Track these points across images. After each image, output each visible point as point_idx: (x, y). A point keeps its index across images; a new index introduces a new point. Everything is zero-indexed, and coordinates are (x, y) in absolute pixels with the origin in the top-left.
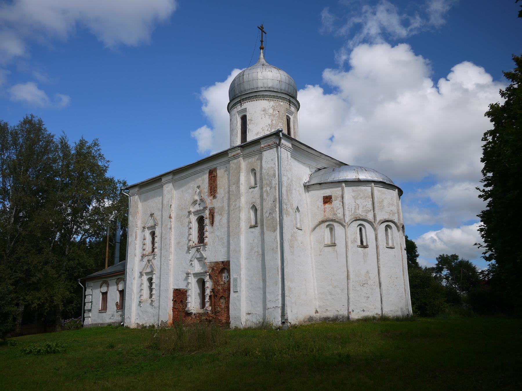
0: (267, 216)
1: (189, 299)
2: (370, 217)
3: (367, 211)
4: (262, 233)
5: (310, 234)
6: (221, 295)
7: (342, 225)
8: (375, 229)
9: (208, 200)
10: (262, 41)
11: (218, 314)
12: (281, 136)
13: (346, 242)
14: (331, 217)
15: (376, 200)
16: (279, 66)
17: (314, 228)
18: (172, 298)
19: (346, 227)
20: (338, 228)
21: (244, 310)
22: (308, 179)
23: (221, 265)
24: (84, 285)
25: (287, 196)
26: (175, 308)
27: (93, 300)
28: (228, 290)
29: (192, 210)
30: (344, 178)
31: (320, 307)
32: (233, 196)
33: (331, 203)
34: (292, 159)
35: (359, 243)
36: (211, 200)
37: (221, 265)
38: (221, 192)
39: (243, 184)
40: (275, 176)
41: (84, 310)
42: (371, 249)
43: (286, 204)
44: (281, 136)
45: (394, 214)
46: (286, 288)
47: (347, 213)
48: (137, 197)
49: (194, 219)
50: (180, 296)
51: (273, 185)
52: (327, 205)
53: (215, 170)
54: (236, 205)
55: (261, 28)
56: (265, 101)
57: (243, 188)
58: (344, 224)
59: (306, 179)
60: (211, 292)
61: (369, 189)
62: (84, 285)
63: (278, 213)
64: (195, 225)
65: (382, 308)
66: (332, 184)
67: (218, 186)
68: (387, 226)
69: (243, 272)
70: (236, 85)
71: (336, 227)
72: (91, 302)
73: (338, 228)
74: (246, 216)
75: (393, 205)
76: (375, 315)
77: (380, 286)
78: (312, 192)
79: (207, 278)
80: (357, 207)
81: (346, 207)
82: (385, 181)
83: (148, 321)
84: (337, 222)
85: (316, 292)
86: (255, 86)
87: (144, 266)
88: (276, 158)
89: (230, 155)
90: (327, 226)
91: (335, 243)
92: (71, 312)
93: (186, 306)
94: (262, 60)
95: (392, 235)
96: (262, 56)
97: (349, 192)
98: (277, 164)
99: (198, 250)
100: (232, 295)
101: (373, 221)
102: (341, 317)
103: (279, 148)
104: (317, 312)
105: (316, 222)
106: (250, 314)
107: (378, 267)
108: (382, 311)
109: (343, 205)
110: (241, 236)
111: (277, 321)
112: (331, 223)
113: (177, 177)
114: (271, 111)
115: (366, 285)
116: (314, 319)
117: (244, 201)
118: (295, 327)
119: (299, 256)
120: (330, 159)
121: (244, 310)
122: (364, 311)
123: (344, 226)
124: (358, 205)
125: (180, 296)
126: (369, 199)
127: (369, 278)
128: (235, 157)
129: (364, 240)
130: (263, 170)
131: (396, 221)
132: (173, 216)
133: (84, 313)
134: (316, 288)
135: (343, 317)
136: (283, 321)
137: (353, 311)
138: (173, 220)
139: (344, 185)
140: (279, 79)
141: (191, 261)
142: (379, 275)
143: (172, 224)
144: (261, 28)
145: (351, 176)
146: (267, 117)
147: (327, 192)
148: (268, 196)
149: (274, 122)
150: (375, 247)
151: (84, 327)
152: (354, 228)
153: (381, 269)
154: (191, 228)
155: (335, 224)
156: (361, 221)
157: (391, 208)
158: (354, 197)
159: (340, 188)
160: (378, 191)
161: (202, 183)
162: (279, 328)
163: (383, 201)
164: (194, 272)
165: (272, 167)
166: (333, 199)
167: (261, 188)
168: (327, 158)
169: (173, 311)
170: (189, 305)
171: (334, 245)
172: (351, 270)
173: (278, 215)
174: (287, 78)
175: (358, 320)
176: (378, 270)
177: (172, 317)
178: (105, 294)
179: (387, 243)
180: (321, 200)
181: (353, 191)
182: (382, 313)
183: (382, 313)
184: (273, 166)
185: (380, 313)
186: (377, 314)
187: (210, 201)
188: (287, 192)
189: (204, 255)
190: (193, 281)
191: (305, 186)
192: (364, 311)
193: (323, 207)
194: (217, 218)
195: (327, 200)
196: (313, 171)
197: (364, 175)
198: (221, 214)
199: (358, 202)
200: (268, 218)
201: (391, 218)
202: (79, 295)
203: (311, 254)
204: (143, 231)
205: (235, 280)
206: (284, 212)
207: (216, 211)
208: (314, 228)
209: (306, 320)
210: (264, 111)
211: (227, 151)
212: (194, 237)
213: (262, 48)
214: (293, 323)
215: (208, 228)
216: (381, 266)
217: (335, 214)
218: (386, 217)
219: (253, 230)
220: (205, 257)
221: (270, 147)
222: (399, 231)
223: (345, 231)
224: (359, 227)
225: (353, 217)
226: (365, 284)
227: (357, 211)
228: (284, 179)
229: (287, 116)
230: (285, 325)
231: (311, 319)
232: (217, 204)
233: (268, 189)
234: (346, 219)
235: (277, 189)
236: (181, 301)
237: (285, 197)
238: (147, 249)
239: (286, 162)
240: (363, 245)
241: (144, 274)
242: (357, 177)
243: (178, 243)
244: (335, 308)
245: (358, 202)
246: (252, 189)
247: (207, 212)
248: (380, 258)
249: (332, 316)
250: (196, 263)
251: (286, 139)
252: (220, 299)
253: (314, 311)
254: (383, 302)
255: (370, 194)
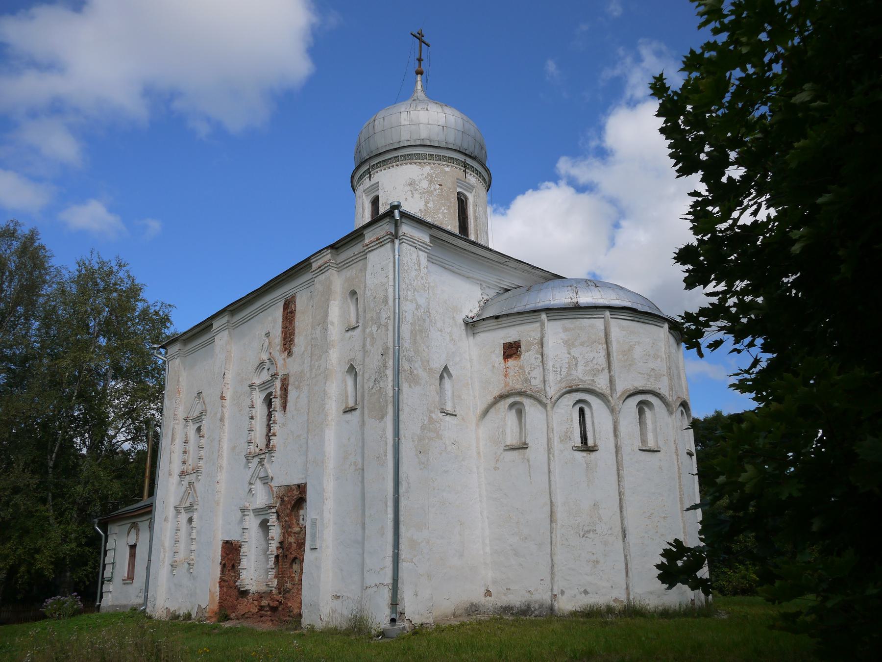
0: (372, 385)
1: (244, 563)
2: (602, 384)
3: (596, 372)
4: (363, 424)
5: (477, 425)
6: (293, 556)
7: (540, 402)
8: (612, 411)
9: (280, 357)
10: (420, 60)
11: (287, 595)
12: (397, 217)
13: (549, 440)
14: (519, 387)
15: (614, 347)
16: (436, 96)
17: (486, 412)
18: (219, 558)
19: (549, 408)
20: (532, 410)
21: (329, 592)
22: (476, 310)
23: (295, 492)
24: (105, 532)
25: (415, 342)
26: (224, 581)
27: (117, 561)
28: (301, 545)
29: (258, 382)
30: (547, 303)
31: (495, 582)
32: (321, 347)
33: (519, 356)
34: (434, 268)
35: (577, 441)
36: (284, 359)
37: (295, 492)
38: (300, 342)
39: (336, 323)
40: (386, 301)
41: (103, 578)
42: (605, 456)
43: (409, 360)
44: (397, 217)
45: (658, 377)
46: (403, 542)
47: (551, 377)
48: (177, 361)
49: (259, 398)
50: (231, 552)
51: (383, 321)
52: (511, 362)
53: (293, 298)
54: (319, 366)
55: (419, 37)
56: (414, 166)
57: (335, 331)
58: (545, 400)
59: (471, 308)
60: (278, 548)
61: (599, 324)
62: (105, 532)
63: (390, 378)
64: (260, 410)
65: (627, 588)
66: (520, 318)
67: (297, 331)
68: (642, 404)
69: (329, 505)
70: (363, 140)
71: (527, 408)
72: (113, 563)
73: (532, 410)
74: (337, 389)
75: (656, 357)
76: (613, 604)
77: (624, 537)
78: (482, 335)
79: (273, 518)
80: (574, 362)
81: (550, 364)
82: (635, 307)
83: (181, 605)
84: (530, 396)
85: (488, 549)
86: (395, 140)
87: (181, 495)
88: (391, 265)
89: (315, 266)
90: (511, 406)
91: (525, 443)
92: (84, 582)
93: (238, 576)
94: (420, 94)
95: (654, 422)
96: (419, 87)
97: (555, 333)
98: (391, 277)
99: (261, 462)
100: (308, 556)
101: (607, 392)
102: (537, 606)
103: (397, 242)
104: (488, 593)
105: (490, 399)
106: (339, 597)
107: (620, 494)
108: (628, 594)
109: (542, 361)
110: (327, 431)
111: (380, 618)
112: (518, 399)
113: (237, 318)
114: (425, 184)
115: (591, 535)
116: (482, 609)
117: (335, 358)
118: (418, 631)
119: (446, 472)
120: (528, 268)
121: (329, 592)
122: (586, 592)
123: (544, 405)
124: (575, 358)
125: (231, 552)
126: (600, 346)
127: (600, 519)
128: (322, 269)
129: (590, 435)
130: (367, 292)
131: (664, 392)
132: (228, 395)
133: (103, 583)
134: (487, 541)
135: (541, 606)
136: (393, 616)
137: (563, 592)
138: (227, 403)
139: (544, 316)
140: (442, 121)
141: (250, 484)
142: (621, 512)
143: (225, 410)
144: (419, 37)
145: (561, 297)
146: (417, 195)
147: (511, 334)
148: (372, 344)
149: (430, 205)
150: (614, 450)
151: (103, 611)
152: (566, 410)
153: (627, 498)
154: (252, 418)
155: (526, 402)
156: (581, 394)
157: (651, 365)
158: (566, 343)
159: (538, 324)
160: (620, 328)
161: (273, 327)
162: (383, 634)
163: (631, 349)
164: (254, 507)
165: (382, 284)
166: (523, 347)
167: (364, 331)
168: (522, 266)
169: (221, 587)
170: (244, 575)
171: (524, 447)
172: (559, 500)
173: (390, 384)
174: (460, 121)
175: (574, 614)
176: (620, 500)
177: (218, 598)
178: (133, 547)
179: (644, 441)
180: (500, 351)
181: (565, 330)
182: (629, 599)
183: (629, 599)
184: (384, 280)
185: (623, 597)
186: (616, 600)
187: (282, 362)
188: (413, 334)
189: (269, 471)
190: (252, 523)
191: (467, 324)
192: (586, 592)
193: (503, 365)
194: (292, 394)
195: (512, 350)
196: (492, 293)
197: (590, 294)
198: (298, 388)
199: (575, 352)
200: (383, 389)
201: (649, 387)
202: (95, 547)
203: (478, 468)
204: (186, 426)
205: (314, 523)
206: (402, 376)
207: (291, 380)
208: (486, 412)
209: (458, 612)
210: (410, 184)
211: (309, 258)
212: (258, 435)
213: (420, 73)
214: (417, 620)
215: (278, 416)
216: (627, 493)
217: (527, 380)
218: (640, 384)
219: (348, 416)
220: (270, 475)
221: (380, 242)
222: (671, 413)
223: (547, 417)
224: (577, 408)
225: (563, 385)
226: (589, 532)
227: (574, 372)
228: (408, 308)
229: (459, 193)
230: (400, 625)
231: (473, 609)
232: (291, 366)
233: (374, 328)
234: (548, 389)
235: (391, 328)
236: (233, 566)
237: (406, 344)
238: (190, 462)
239: (414, 273)
240: (585, 446)
241: (183, 511)
242: (575, 300)
243: (233, 448)
244: (525, 587)
245: (575, 352)
246: (350, 333)
247: (278, 384)
248: (625, 472)
249: (518, 604)
250: (259, 488)
251: (415, 224)
252: (291, 564)
253: (483, 591)
254: (630, 574)
255: (602, 335)
